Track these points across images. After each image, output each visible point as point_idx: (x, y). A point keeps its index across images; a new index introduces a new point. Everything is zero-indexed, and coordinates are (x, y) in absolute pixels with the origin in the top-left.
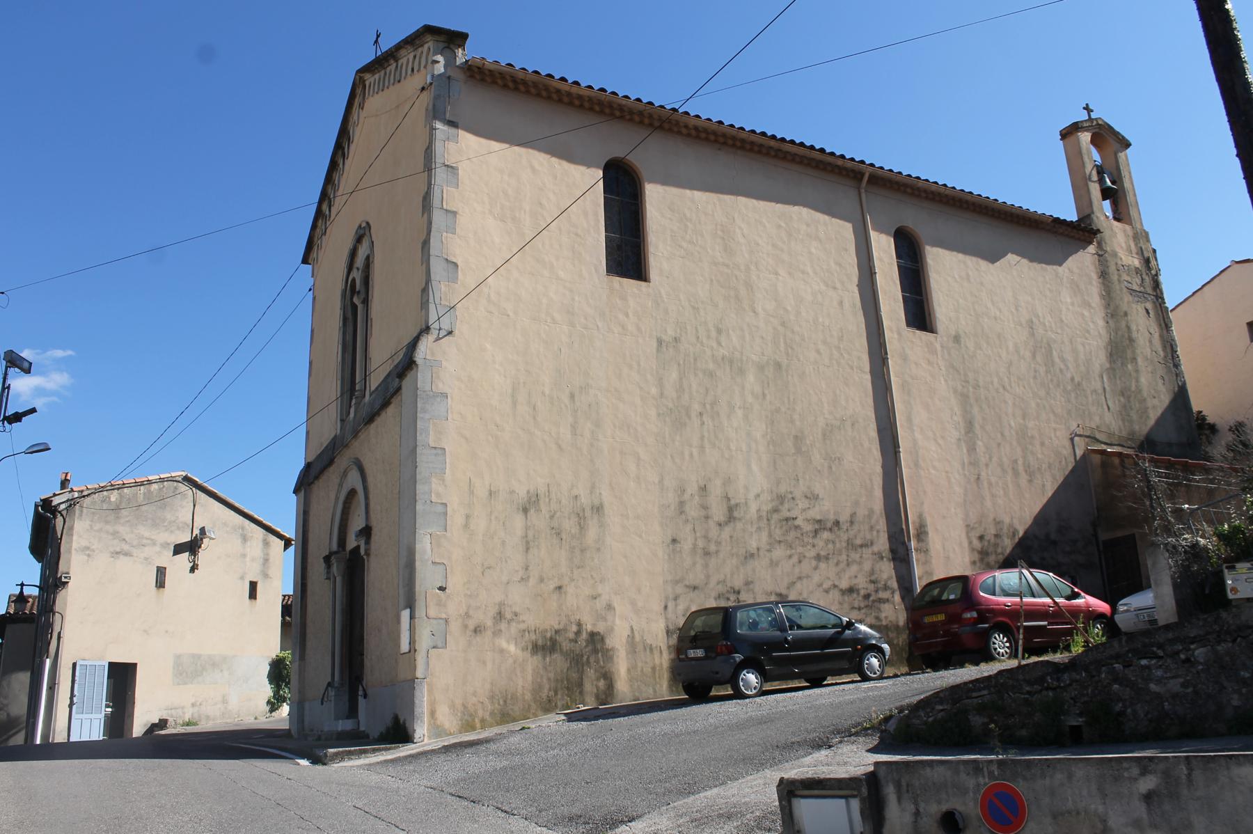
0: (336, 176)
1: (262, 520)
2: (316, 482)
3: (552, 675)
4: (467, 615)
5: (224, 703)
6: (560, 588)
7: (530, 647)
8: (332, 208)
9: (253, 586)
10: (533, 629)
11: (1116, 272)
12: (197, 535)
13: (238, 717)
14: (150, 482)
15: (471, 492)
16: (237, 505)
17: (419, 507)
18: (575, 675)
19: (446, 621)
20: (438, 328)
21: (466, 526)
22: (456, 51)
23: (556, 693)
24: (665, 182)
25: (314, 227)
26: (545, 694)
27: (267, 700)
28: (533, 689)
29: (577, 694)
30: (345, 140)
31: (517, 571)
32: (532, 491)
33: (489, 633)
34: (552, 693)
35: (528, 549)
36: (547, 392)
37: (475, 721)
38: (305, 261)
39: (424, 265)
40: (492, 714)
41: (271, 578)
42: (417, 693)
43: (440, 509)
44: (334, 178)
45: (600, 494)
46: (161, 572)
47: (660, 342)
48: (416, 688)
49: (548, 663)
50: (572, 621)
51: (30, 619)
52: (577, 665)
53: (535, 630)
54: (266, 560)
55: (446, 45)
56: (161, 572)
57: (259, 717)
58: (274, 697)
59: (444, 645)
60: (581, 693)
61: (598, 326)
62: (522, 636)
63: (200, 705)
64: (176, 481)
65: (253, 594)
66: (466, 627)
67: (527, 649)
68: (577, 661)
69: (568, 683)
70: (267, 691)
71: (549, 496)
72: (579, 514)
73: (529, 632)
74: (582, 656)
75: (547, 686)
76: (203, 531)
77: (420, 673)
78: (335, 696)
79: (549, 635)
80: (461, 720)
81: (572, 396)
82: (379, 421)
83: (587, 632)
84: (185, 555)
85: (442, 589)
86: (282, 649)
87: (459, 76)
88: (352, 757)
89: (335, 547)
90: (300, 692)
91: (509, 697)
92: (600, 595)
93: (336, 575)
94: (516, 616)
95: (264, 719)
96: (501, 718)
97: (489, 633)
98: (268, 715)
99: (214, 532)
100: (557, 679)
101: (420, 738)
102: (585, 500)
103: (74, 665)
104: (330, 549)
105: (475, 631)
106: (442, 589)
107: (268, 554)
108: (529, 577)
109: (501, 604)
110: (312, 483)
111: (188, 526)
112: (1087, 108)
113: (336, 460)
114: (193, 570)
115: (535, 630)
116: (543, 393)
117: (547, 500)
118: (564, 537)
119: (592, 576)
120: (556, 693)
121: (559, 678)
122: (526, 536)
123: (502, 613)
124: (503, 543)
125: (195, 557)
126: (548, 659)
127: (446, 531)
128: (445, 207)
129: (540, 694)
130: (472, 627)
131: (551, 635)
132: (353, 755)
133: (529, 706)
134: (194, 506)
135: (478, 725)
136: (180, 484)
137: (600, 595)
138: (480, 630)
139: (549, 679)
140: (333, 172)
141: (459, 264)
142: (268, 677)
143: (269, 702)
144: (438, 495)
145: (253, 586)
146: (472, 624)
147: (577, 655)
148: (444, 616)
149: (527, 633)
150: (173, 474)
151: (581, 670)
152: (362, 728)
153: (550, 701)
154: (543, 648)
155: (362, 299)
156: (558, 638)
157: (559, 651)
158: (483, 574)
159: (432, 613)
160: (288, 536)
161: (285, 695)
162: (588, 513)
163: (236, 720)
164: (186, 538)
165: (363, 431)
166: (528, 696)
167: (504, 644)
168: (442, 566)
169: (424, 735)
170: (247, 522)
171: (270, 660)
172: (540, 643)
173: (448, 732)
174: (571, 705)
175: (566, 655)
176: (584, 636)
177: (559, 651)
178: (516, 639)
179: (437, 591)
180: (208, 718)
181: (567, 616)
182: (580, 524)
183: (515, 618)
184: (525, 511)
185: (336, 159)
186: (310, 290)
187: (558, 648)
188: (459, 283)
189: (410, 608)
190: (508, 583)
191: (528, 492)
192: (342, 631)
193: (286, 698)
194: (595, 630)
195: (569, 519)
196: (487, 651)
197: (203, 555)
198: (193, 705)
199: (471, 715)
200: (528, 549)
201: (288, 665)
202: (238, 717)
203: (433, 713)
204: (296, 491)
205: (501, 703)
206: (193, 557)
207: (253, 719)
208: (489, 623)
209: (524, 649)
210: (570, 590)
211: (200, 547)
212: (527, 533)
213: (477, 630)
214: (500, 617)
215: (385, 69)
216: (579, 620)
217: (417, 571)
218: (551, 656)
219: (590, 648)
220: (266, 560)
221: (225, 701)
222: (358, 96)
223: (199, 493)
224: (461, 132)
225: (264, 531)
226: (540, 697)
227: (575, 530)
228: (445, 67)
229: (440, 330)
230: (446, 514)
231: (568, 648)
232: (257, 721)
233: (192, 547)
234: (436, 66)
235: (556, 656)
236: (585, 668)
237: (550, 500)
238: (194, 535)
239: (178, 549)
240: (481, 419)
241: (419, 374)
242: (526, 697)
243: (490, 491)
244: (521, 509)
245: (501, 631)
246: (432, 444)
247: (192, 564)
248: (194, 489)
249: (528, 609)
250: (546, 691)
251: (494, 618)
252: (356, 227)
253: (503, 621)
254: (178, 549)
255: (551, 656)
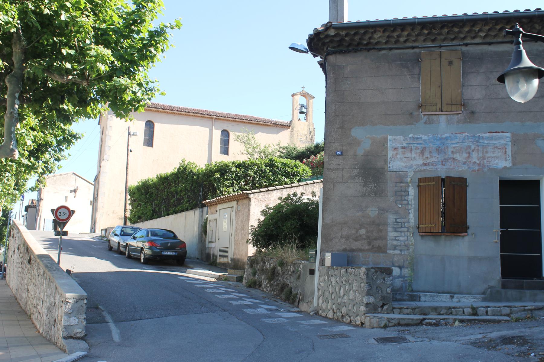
11: (297, 136)
14: (64, 175)
24: (158, 123)
38: (99, 124)
46: (66, 197)
47: (154, 160)
51: (34, 207)
56: (66, 197)
76: (77, 187)
84: (73, 193)
103: (45, 219)
112: (303, 87)
114: (75, 197)
164: (73, 189)
184: (120, 194)
197: (77, 193)
233: (75, 191)
239: (71, 191)
254: (71, 191)
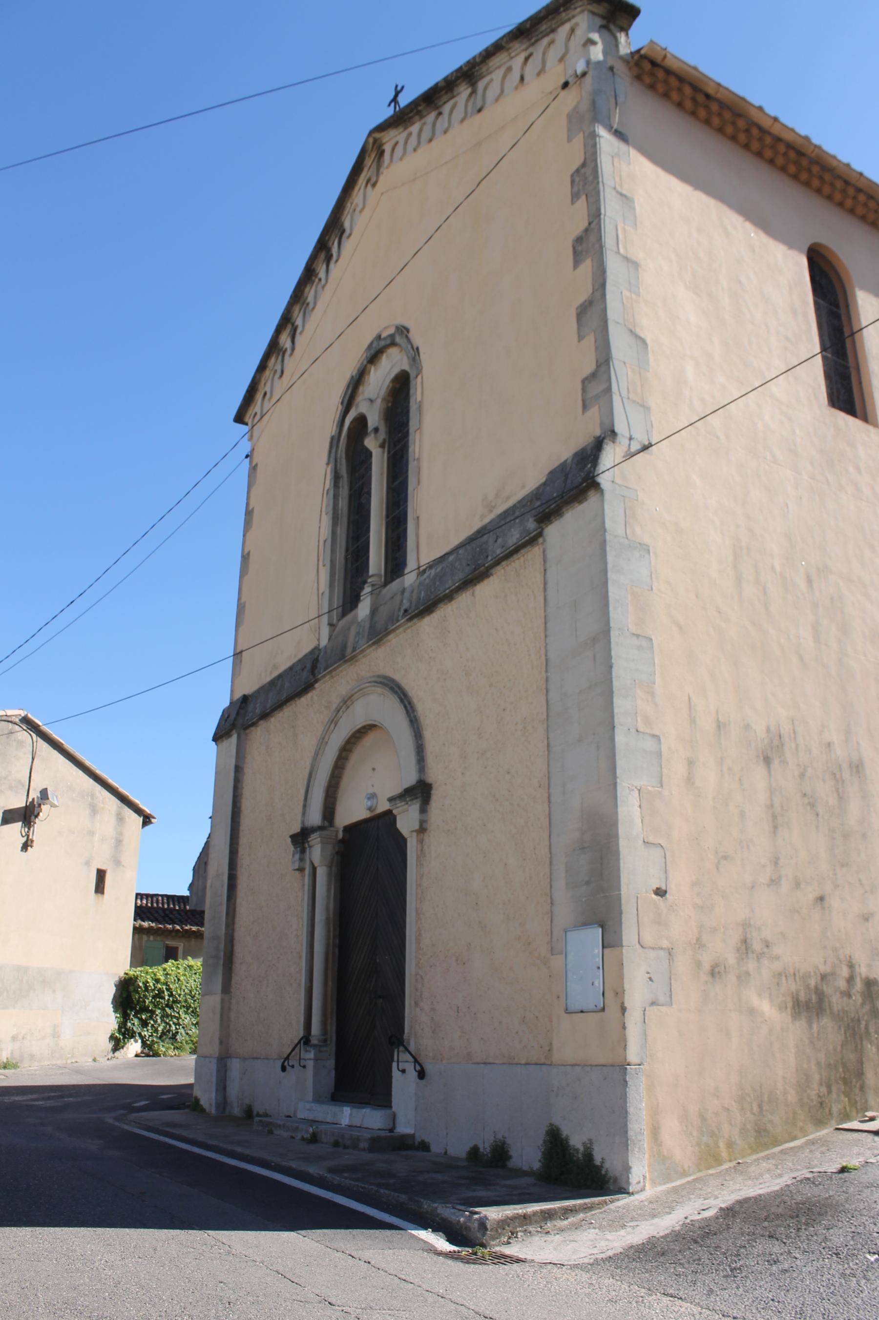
0: (310, 293)
1: (118, 786)
2: (261, 722)
3: (822, 1056)
4: (699, 944)
5: (54, 1037)
6: (821, 899)
7: (790, 1005)
8: (298, 337)
9: (101, 875)
10: (792, 971)
12: (33, 799)
13: (72, 1057)
15: (693, 721)
16: (88, 763)
17: (620, 738)
18: (852, 1057)
19: (670, 953)
20: (628, 436)
21: (689, 780)
22: (618, 35)
23: (829, 1087)
25: (262, 367)
26: (814, 1092)
27: (110, 1035)
28: (798, 1082)
29: (857, 1091)
30: (333, 236)
31: (764, 866)
32: (772, 728)
33: (732, 978)
34: (824, 1090)
35: (775, 828)
36: (778, 568)
37: (718, 1147)
38: (239, 418)
39: (590, 341)
40: (743, 1131)
41: (123, 866)
42: (631, 1092)
43: (649, 744)
44: (305, 294)
45: (858, 743)
48: (629, 1083)
49: (816, 1035)
50: (842, 957)
52: (854, 1038)
53: (794, 974)
54: (119, 842)
55: (604, 22)
57: (98, 1059)
58: (120, 1028)
59: (668, 999)
60: (862, 1088)
61: (827, 480)
62: (778, 984)
63: (23, 1038)
64: (11, 722)
65: (100, 888)
66: (698, 964)
67: (786, 1008)
68: (854, 1030)
69: (844, 1071)
70: (111, 1021)
71: (795, 738)
72: (835, 774)
73: (786, 976)
74: (859, 1021)
75: (817, 1077)
76: (44, 794)
77: (633, 1054)
78: (316, 1059)
79: (812, 983)
80: (698, 1144)
81: (809, 581)
82: (447, 612)
83: (861, 978)
85: (660, 892)
86: (133, 965)
87: (620, 67)
88: (531, 1229)
89: (315, 818)
90: (221, 1042)
91: (766, 1098)
92: (872, 915)
93: (316, 864)
94: (767, 946)
95: (103, 1062)
96: (756, 1139)
97: (732, 978)
98: (111, 1055)
99: (57, 797)
100: (830, 1065)
101: (639, 1182)
102: (839, 752)
104: (303, 822)
105: (712, 973)
106: (660, 892)
107: (121, 834)
108: (780, 878)
109: (746, 925)
110: (254, 724)
111: (23, 786)
113: (317, 685)
114: (25, 847)
115: (794, 974)
116: (773, 568)
117: (793, 746)
118: (820, 811)
119: (860, 880)
120: (830, 1092)
121: (832, 1062)
122: (772, 806)
123: (748, 941)
124: (742, 814)
125: (29, 829)
126: (815, 1026)
127: (662, 786)
128: (622, 251)
129: (809, 1091)
130: (707, 967)
131: (816, 983)
132: (531, 1224)
133: (795, 1113)
134: (33, 759)
135: (724, 1155)
136: (17, 727)
137: (872, 915)
138: (719, 973)
139: (818, 1064)
140: (306, 286)
141: (648, 341)
142: (112, 1003)
143: (112, 1038)
144: (647, 720)
145: (101, 875)
146: (707, 960)
147: (852, 1020)
148: (665, 944)
149: (784, 978)
150: (9, 713)
151: (859, 1046)
152: (404, 1128)
153: (821, 1104)
154: (807, 1006)
155: (381, 440)
156: (825, 989)
157: (828, 1011)
158: (718, 869)
159: (648, 937)
160: (148, 811)
161: (135, 1029)
162: (846, 774)
163: (69, 1061)
164: (19, 802)
165: (401, 630)
166: (792, 1097)
167: (755, 1001)
168: (660, 850)
169: (644, 1177)
170: (98, 787)
171: (117, 979)
172: (802, 997)
173: (680, 1169)
174: (850, 1111)
175: (838, 1018)
176: (859, 985)
177: (828, 1011)
178: (769, 988)
179: (654, 896)
180: (32, 1057)
181: (835, 950)
182: (837, 790)
183: (765, 950)
184: (767, 761)
185: (314, 266)
186: (247, 456)
187: (827, 1004)
188: (651, 370)
189: (602, 926)
190: (753, 887)
191: (768, 730)
192: (327, 954)
193: (134, 1032)
194: (872, 976)
195: (824, 781)
196: (730, 1010)
197: (40, 826)
198: (14, 1039)
199: (713, 1134)
200: (775, 828)
201: (140, 987)
202: (72, 1057)
203: (655, 1132)
204: (217, 738)
205: (755, 1108)
206: (26, 830)
207: (91, 1060)
208: (731, 959)
209: (782, 1008)
210: (834, 902)
211: (37, 816)
212: (772, 800)
213: (715, 972)
214: (747, 949)
215: (437, 108)
216: (850, 957)
217: (621, 856)
218: (818, 1021)
219: (867, 1007)
220: (119, 842)
221: (56, 1034)
222: (366, 170)
223: (41, 742)
224: (633, 153)
225: (119, 802)
226: (809, 1097)
227: (832, 801)
228: (605, 52)
229: (631, 439)
230: (659, 754)
231: (840, 1007)
232: (97, 1064)
234: (592, 48)
235: (826, 1021)
236: (865, 1042)
237: (797, 746)
238: (30, 800)
240: (697, 597)
241: (606, 507)
242: (790, 1098)
243: (718, 721)
244: (762, 758)
245: (748, 973)
246: (633, 629)
247: (25, 839)
248: (34, 735)
249: (783, 935)
250: (815, 1085)
251: (738, 950)
252: (374, 336)
253: (750, 955)
255: (818, 1021)
